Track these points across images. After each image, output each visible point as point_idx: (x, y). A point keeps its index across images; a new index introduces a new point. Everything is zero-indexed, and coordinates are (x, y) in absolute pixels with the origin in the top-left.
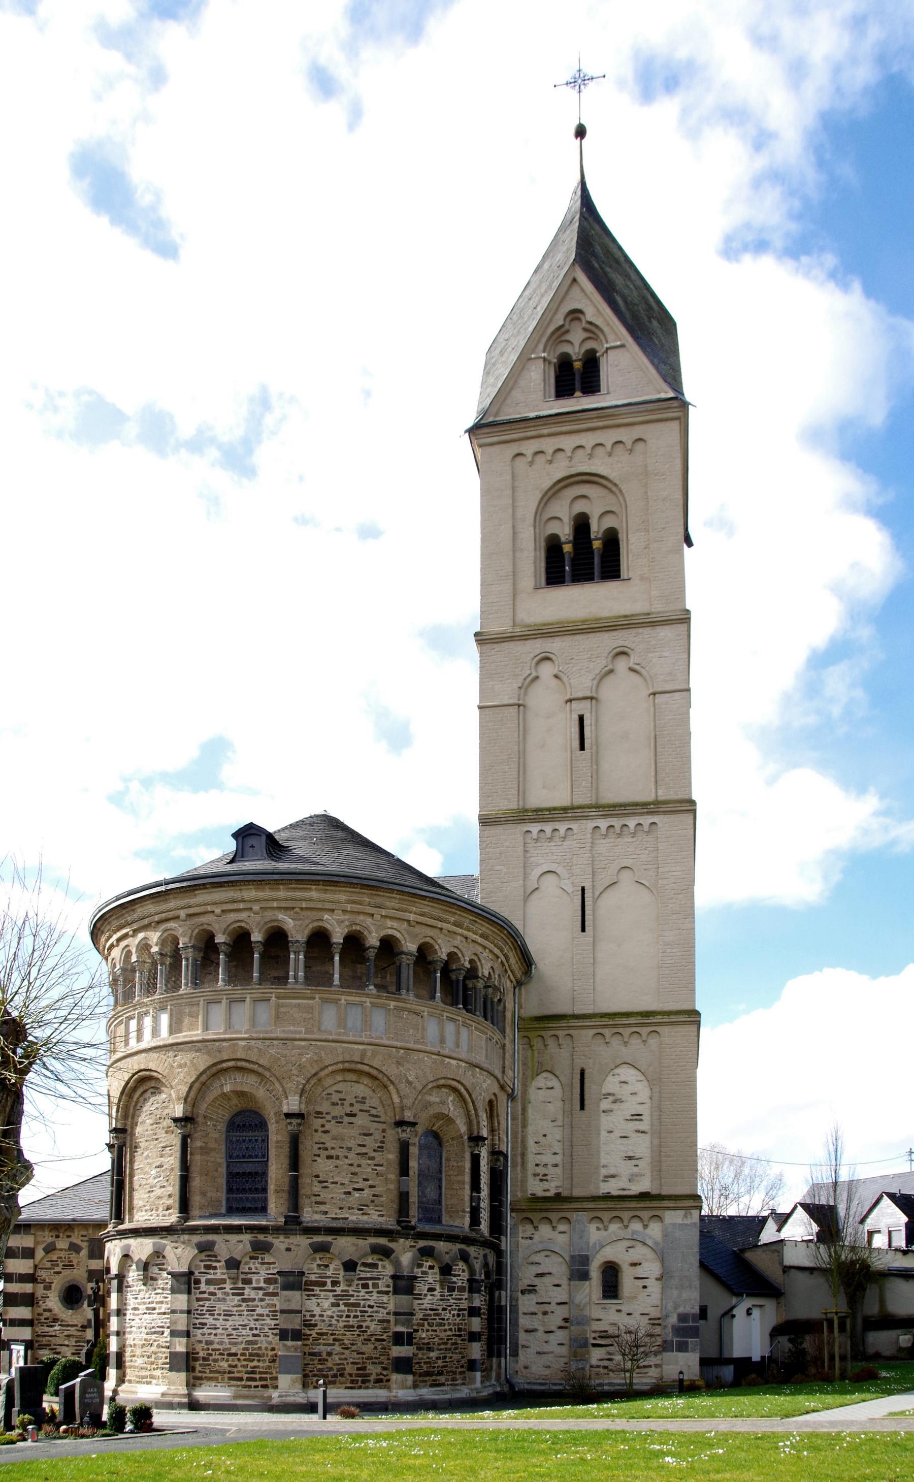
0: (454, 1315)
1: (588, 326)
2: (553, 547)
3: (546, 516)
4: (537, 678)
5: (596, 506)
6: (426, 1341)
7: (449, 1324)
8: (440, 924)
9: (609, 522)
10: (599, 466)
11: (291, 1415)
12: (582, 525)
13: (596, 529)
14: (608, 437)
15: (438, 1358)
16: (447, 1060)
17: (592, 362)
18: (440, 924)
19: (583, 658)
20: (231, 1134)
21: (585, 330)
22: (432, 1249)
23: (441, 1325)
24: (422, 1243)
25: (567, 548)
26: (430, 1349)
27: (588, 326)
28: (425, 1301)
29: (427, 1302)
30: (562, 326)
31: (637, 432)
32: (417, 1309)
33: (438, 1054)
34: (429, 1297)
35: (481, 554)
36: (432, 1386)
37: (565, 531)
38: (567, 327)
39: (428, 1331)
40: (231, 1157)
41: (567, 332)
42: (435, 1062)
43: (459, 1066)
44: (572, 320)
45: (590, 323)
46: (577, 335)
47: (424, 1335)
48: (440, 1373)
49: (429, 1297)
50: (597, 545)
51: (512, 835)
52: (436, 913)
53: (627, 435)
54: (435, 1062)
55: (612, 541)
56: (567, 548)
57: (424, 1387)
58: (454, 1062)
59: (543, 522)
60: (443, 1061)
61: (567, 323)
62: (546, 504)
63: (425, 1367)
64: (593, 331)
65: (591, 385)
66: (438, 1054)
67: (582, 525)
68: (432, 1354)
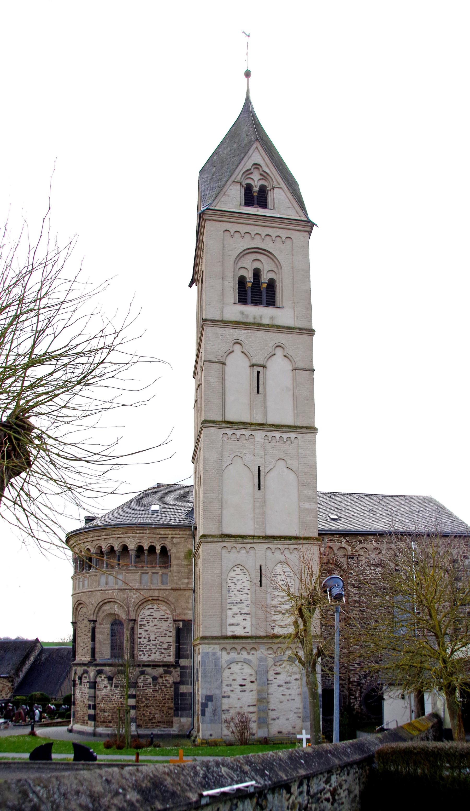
0: (118, 698)
1: (262, 173)
2: (242, 282)
3: (240, 265)
4: (233, 352)
6: (103, 708)
7: (115, 701)
8: (100, 538)
10: (268, 245)
12: (257, 274)
13: (265, 278)
14: (273, 232)
15: (109, 716)
16: (107, 591)
17: (263, 191)
18: (100, 538)
19: (258, 342)
21: (261, 175)
22: (102, 670)
23: (110, 702)
24: (98, 668)
26: (105, 712)
27: (262, 173)
28: (103, 692)
29: (104, 692)
30: (250, 170)
31: (289, 233)
32: (99, 695)
33: (102, 590)
34: (104, 690)
36: (106, 727)
37: (249, 277)
39: (104, 704)
41: (252, 173)
42: (102, 594)
43: (113, 593)
45: (263, 171)
46: (256, 176)
47: (102, 706)
48: (110, 722)
49: (104, 690)
51: (215, 434)
52: (96, 534)
53: (284, 234)
54: (102, 594)
55: (272, 284)
56: (249, 285)
57: (102, 727)
58: (111, 591)
59: (237, 269)
60: (105, 592)
61: (253, 168)
62: (243, 256)
63: (102, 719)
64: (264, 176)
65: (263, 204)
66: (102, 590)
67: (257, 274)
68: (105, 714)
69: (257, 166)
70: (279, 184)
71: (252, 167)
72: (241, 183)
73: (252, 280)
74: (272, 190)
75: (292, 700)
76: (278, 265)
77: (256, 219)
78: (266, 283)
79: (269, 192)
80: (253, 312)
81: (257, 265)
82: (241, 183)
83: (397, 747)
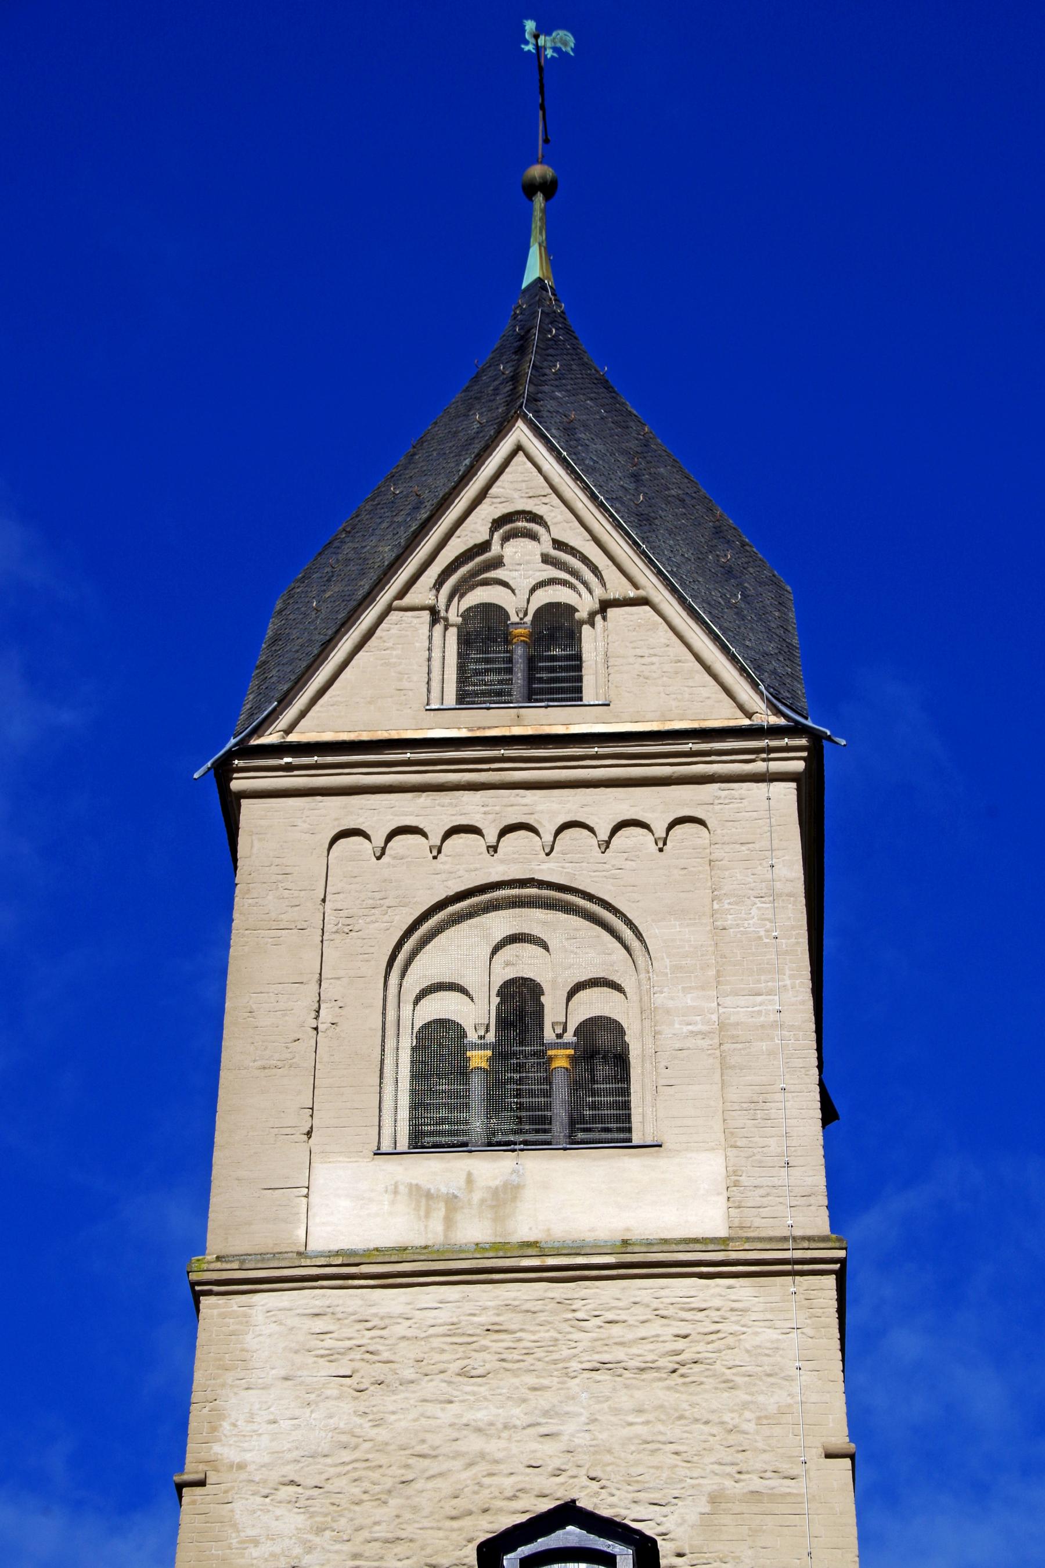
2: (438, 1050)
5: (563, 956)
9: (593, 1004)
10: (574, 864)
11: (585, 731)
12: (520, 1002)
13: (560, 1017)
14: (604, 807)
17: (557, 628)
20: (560, 1113)
21: (546, 559)
25: (478, 1059)
30: (485, 546)
35: (228, 946)
37: (475, 1015)
38: (495, 548)
40: (542, 1123)
44: (506, 539)
45: (558, 544)
50: (561, 1060)
53: (655, 805)
55: (603, 1052)
56: (478, 1059)
59: (409, 996)
67: (520, 1002)
69: (515, 524)
70: (636, 586)
71: (492, 532)
72: (433, 611)
73: (491, 1037)
74: (598, 618)
75: (317, 1018)
76: (627, 934)
77: (505, 703)
78: (566, 1046)
79: (586, 629)
80: (568, 1195)
81: (524, 962)
82: (433, 611)
83: (765, 770)
